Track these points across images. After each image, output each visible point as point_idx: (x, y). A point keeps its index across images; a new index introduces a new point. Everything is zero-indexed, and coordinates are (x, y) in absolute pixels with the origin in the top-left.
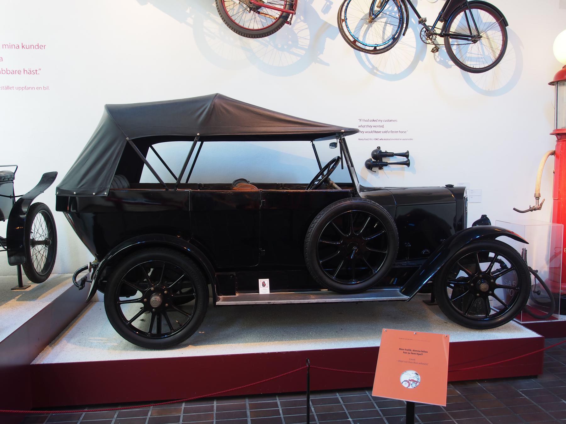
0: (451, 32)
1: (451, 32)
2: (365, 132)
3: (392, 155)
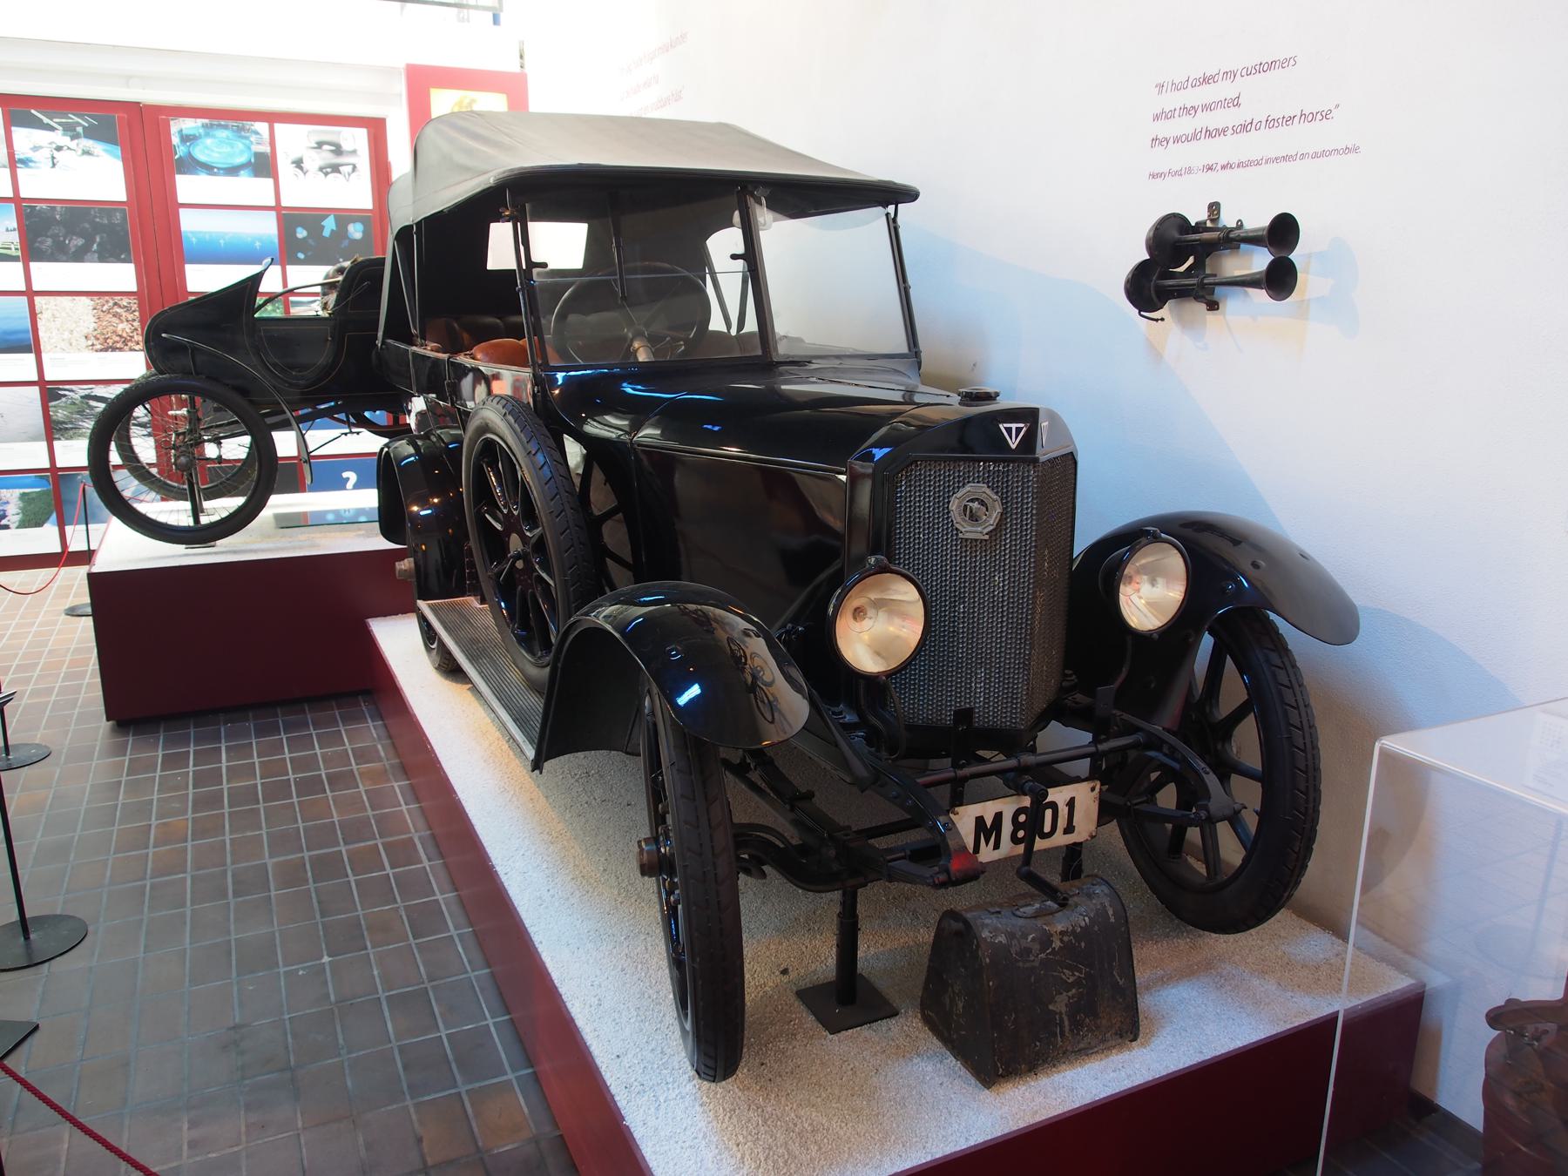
0: (751, 256)
1: (751, 256)
2: (1172, 140)
3: (1232, 240)
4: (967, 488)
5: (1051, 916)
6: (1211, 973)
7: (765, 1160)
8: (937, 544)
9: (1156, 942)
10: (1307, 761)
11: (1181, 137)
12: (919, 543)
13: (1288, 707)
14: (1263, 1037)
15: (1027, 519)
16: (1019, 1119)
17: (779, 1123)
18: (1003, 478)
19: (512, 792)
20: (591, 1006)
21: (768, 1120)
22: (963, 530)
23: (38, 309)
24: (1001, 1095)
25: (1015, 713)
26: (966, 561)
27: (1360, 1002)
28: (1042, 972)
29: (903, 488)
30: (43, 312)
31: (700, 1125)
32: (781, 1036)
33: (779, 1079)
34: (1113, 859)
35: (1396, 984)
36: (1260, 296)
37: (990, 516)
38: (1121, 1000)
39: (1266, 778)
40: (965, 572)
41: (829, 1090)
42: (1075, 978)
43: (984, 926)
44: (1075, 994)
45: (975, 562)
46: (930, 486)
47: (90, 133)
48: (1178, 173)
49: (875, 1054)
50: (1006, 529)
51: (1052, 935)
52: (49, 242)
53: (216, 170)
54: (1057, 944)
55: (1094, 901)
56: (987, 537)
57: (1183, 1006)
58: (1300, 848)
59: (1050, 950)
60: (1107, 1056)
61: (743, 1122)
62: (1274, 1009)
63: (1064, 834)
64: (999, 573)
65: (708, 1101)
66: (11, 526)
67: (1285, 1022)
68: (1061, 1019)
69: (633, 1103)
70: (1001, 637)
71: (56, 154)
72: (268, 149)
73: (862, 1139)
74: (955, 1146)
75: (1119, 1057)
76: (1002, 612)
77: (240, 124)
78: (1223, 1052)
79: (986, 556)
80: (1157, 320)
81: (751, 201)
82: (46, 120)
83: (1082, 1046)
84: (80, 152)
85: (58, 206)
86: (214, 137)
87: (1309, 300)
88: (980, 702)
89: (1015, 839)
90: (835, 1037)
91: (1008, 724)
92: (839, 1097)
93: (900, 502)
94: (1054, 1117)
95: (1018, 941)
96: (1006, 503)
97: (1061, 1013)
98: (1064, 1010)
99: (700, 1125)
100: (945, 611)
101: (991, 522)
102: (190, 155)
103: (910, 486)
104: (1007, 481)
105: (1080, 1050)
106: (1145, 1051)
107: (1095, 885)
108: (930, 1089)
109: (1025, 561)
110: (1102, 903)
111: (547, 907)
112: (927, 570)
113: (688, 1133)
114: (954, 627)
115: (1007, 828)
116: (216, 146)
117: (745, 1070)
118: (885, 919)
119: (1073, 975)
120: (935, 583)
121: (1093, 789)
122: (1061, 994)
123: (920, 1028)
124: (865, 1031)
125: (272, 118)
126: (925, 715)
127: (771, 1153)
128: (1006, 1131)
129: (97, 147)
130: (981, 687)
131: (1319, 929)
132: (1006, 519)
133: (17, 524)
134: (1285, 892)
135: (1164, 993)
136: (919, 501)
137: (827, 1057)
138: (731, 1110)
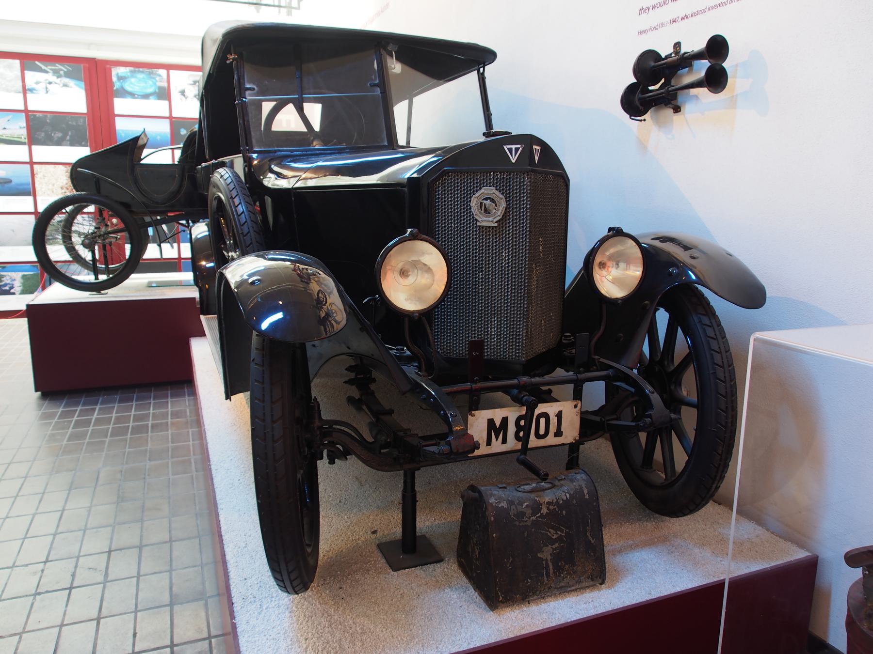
2: (651, 8)
3: (686, 61)
4: (482, 191)
5: (542, 492)
6: (666, 544)
7: (322, 650)
8: (463, 230)
9: (632, 523)
10: (726, 389)
11: (657, 4)
12: (451, 230)
13: (713, 352)
14: (697, 586)
15: (523, 212)
16: (510, 632)
17: (340, 626)
18: (506, 183)
19: (238, 426)
20: (239, 548)
21: (332, 624)
22: (480, 220)
23: (35, 172)
24: (501, 616)
25: (519, 349)
26: (482, 242)
27: (770, 566)
28: (533, 530)
29: (440, 192)
30: (38, 173)
31: (285, 625)
32: (359, 570)
33: (349, 598)
34: (612, 474)
35: (799, 554)
36: (703, 91)
37: (498, 210)
38: (592, 554)
39: (700, 406)
40: (482, 250)
41: (381, 607)
42: (558, 535)
43: (491, 495)
44: (558, 547)
45: (489, 242)
46: (458, 190)
47: (68, 75)
48: (655, 28)
49: (421, 586)
50: (509, 219)
51: (541, 504)
52: (43, 134)
53: (136, 96)
54: (544, 511)
55: (574, 484)
56: (496, 225)
57: (643, 564)
58: (722, 451)
59: (540, 514)
60: (582, 593)
61: (315, 625)
62: (707, 568)
63: (555, 436)
64: (505, 250)
65: (296, 610)
66: (16, 293)
67: (714, 576)
68: (547, 564)
69: (244, 609)
70: (508, 295)
71: (48, 86)
72: (166, 85)
73: (395, 640)
74: (459, 648)
75: (591, 594)
76: (508, 277)
77: (150, 70)
78: (666, 594)
79: (496, 238)
80: (641, 121)
81: (383, 52)
82: (43, 67)
83: (562, 584)
84: (61, 85)
85: (49, 115)
86: (136, 77)
87: (737, 95)
88: (494, 341)
89: (517, 436)
90: (395, 573)
91: (514, 357)
92: (387, 612)
93: (438, 202)
94: (536, 631)
95: (516, 507)
96: (509, 201)
97: (547, 560)
98: (549, 557)
99: (285, 625)
100: (470, 277)
101: (499, 214)
102: (122, 88)
103: (445, 190)
104: (509, 186)
105: (561, 587)
106: (610, 591)
107: (577, 474)
108: (452, 609)
109: (523, 242)
110: (579, 485)
111: (234, 489)
112: (457, 249)
113: (275, 630)
114: (475, 288)
115: (512, 429)
116: (137, 82)
117: (328, 592)
118: (451, 503)
119: (557, 534)
120: (462, 258)
121: (576, 406)
122: (547, 546)
123: (456, 570)
124: (418, 571)
125: (169, 67)
126: (457, 351)
127: (327, 647)
128: (499, 639)
129: (71, 83)
130: (494, 331)
131: (746, 520)
132: (509, 212)
133: (19, 292)
134: (713, 483)
135: (630, 555)
136: (451, 201)
137: (386, 586)
138: (309, 616)
